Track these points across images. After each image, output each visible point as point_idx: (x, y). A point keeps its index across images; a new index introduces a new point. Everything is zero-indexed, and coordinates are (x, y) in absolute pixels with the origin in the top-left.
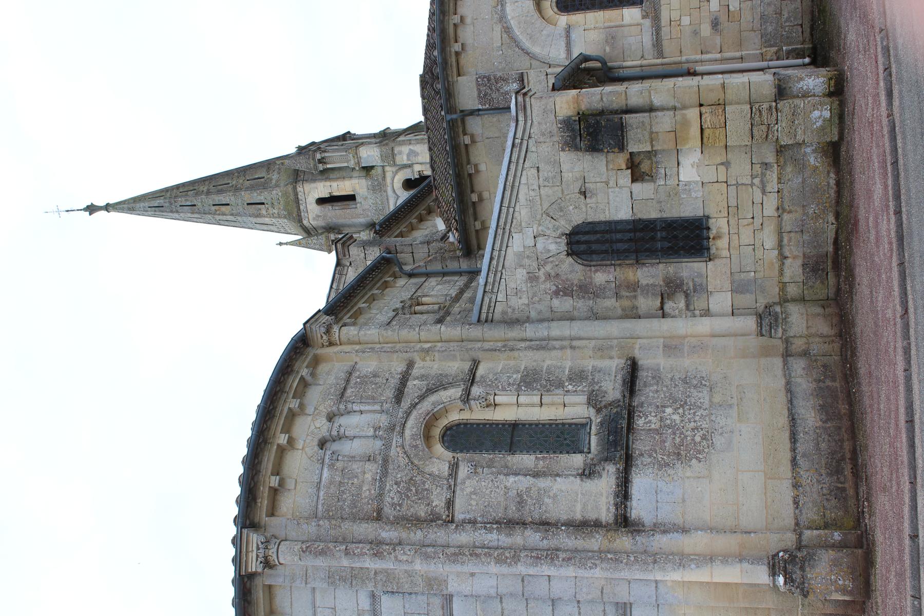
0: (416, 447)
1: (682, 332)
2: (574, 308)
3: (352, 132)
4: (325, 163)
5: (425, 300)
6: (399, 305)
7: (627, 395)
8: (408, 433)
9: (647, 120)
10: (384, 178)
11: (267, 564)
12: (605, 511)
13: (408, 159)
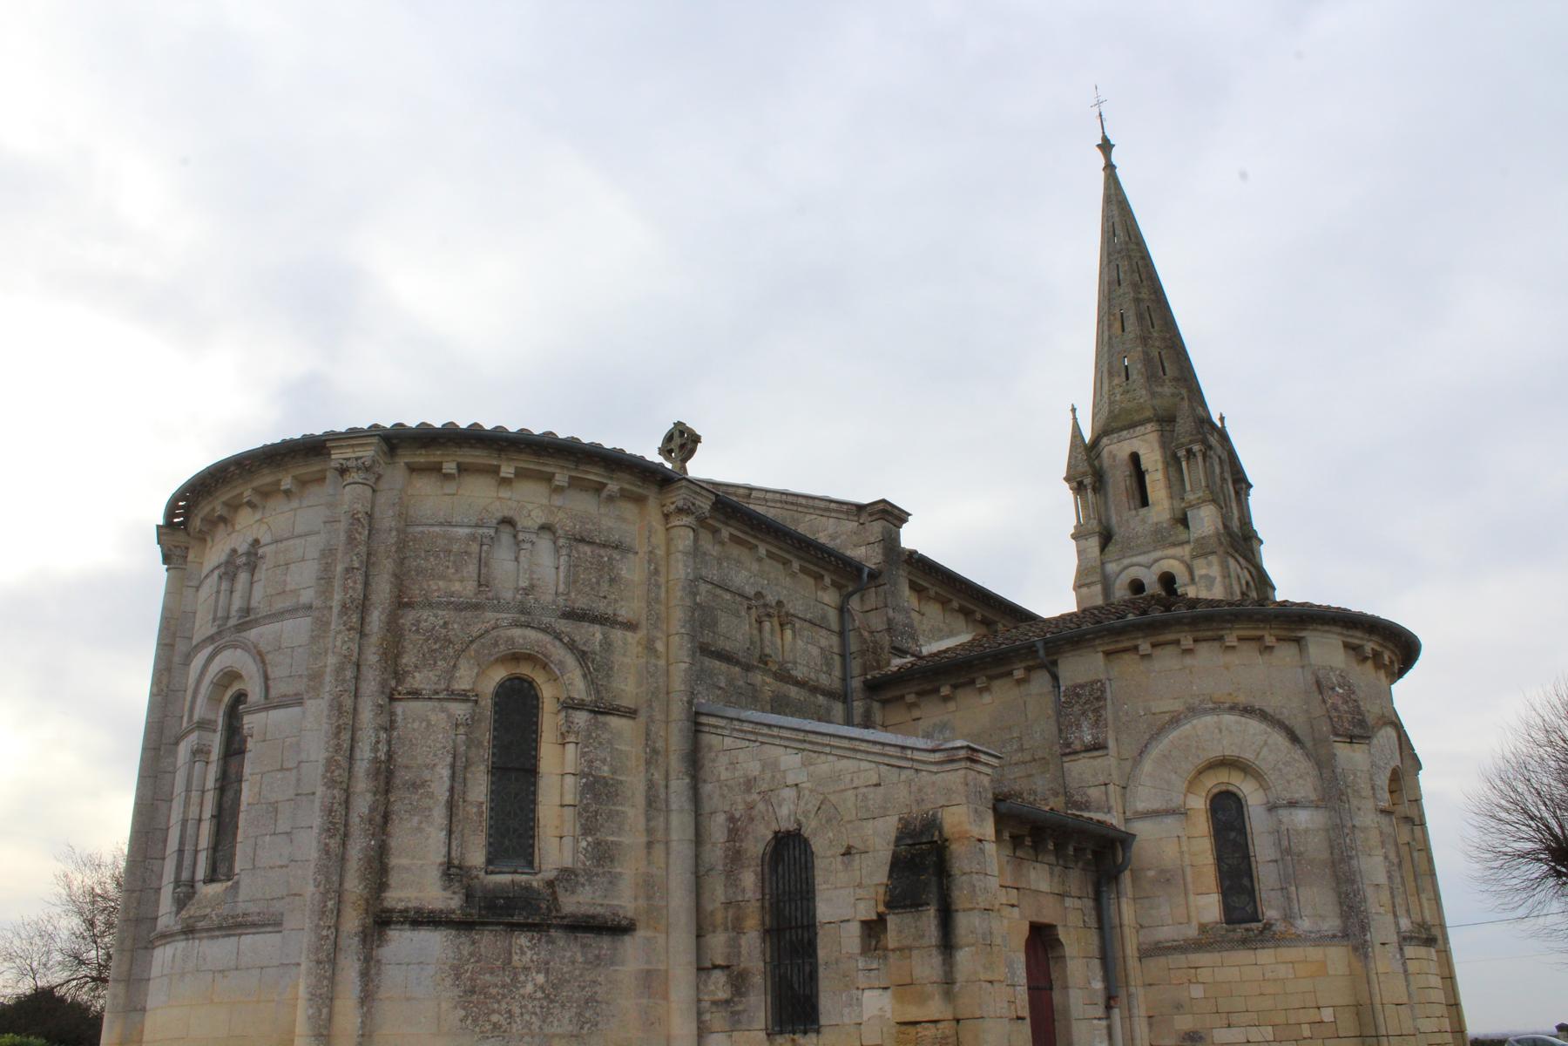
0: (496, 644)
1: (673, 996)
2: (714, 845)
3: (1252, 491)
4: (1188, 459)
5: (788, 633)
6: (771, 599)
7: (565, 922)
8: (517, 632)
9: (925, 942)
10: (1174, 545)
11: (343, 471)
12: (399, 896)
13: (1201, 577)
